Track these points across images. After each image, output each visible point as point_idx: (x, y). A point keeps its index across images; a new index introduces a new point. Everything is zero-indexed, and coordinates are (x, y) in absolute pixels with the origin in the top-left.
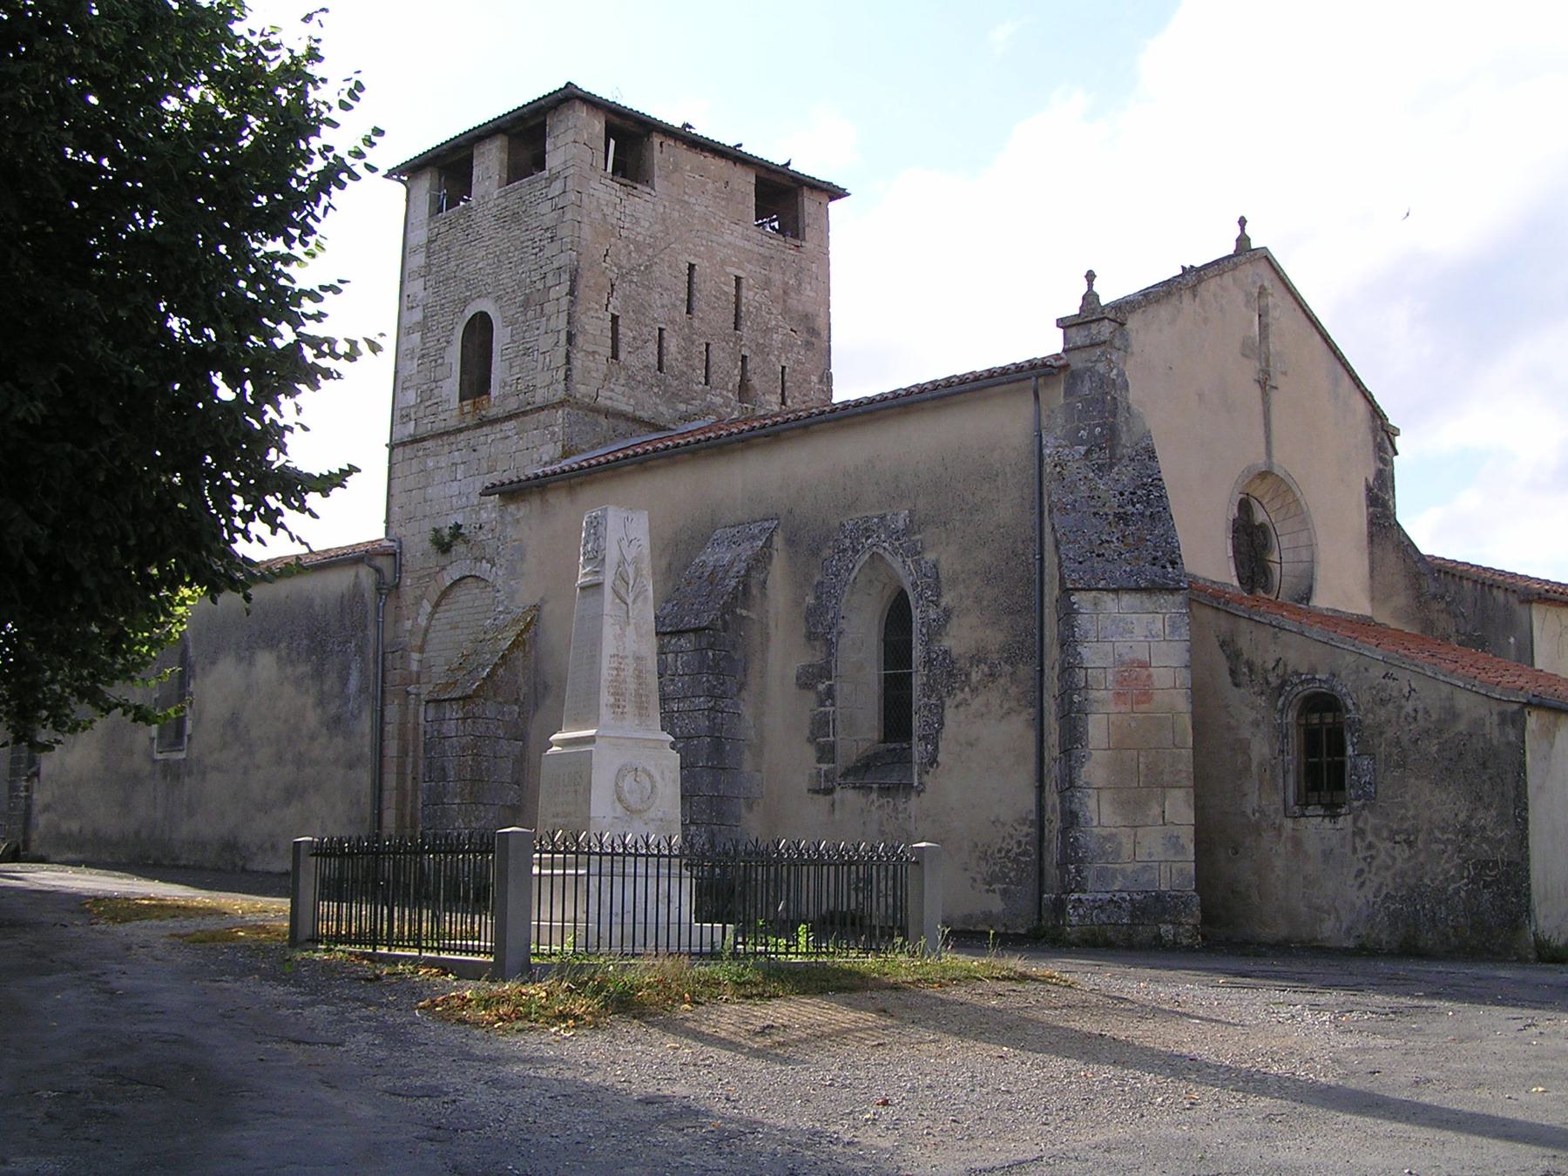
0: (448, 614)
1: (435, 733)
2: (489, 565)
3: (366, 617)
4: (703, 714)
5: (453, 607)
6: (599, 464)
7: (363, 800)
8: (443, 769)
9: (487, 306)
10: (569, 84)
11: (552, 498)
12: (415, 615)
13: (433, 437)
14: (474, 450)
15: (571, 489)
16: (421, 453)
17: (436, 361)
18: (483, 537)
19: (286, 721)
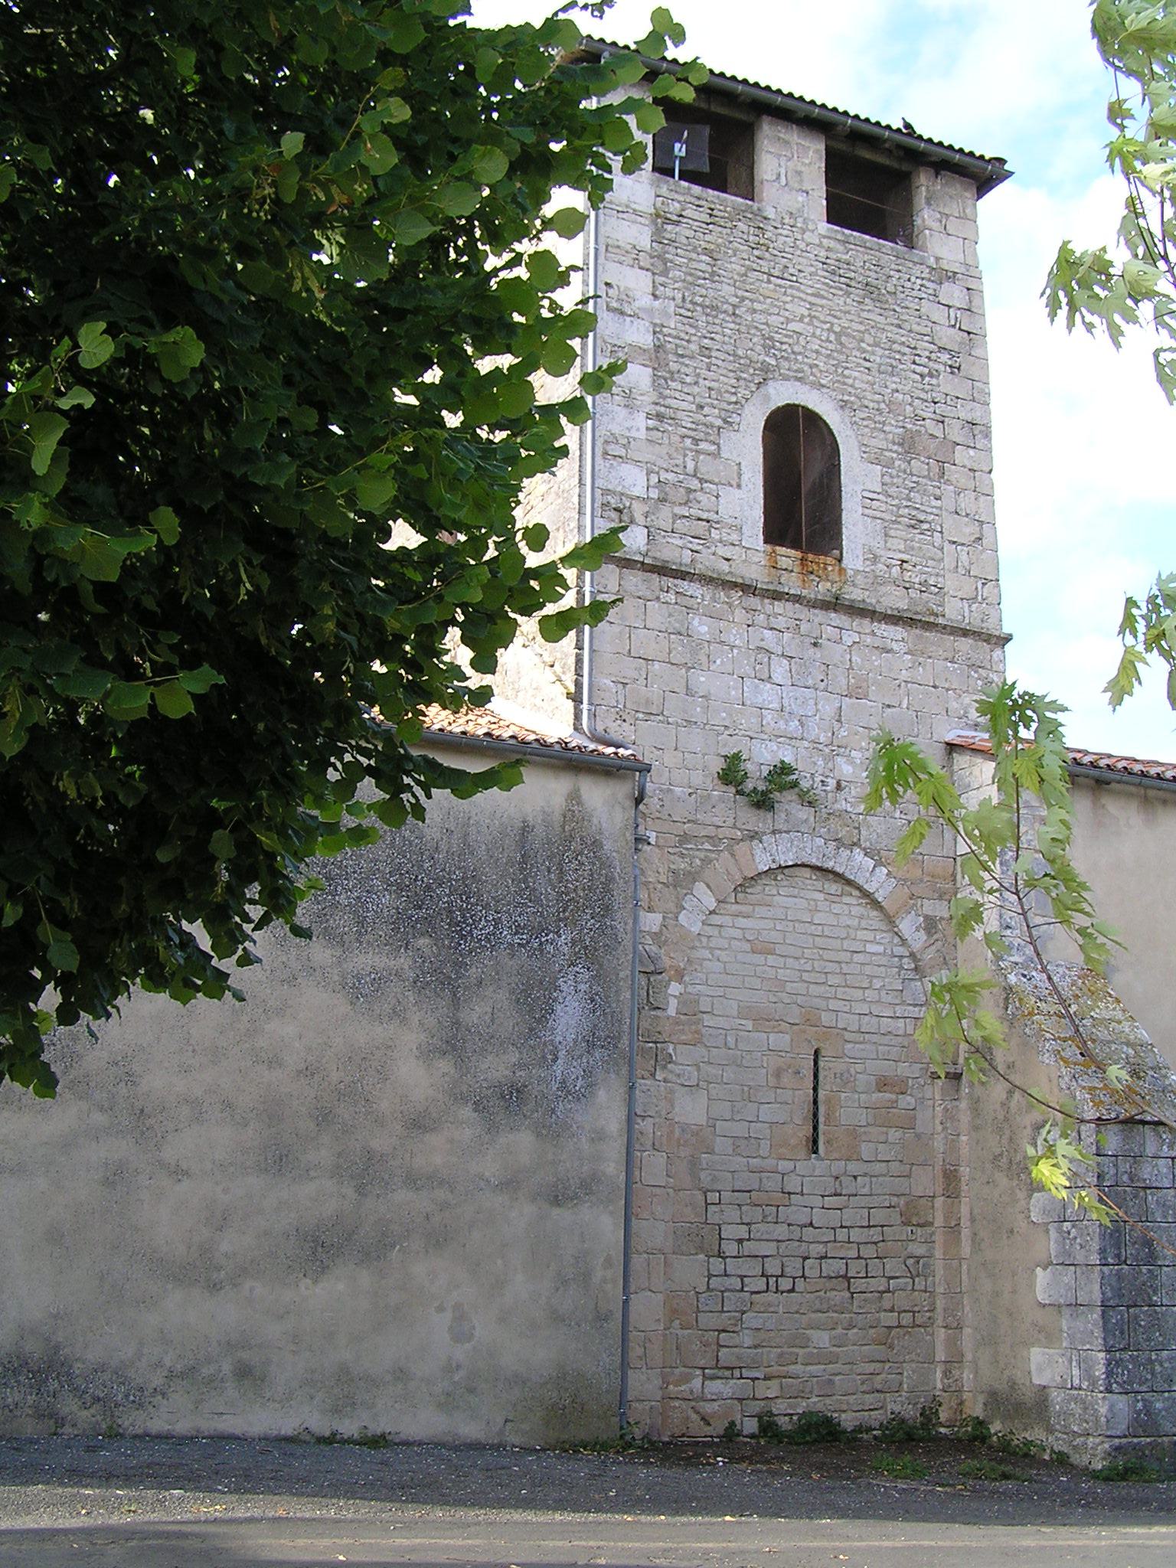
0: (742, 922)
1: (1125, 1178)
2: (871, 863)
3: (607, 890)
4: (569, 1101)
5: (761, 911)
6: (1159, 776)
7: (598, 1274)
8: (1148, 1243)
9: (783, 393)
10: (527, 23)
11: (1113, 806)
12: (671, 906)
13: (707, 580)
14: (815, 645)
15: (1146, 802)
16: (671, 597)
17: (696, 441)
18: (843, 805)
19: (308, 1072)
